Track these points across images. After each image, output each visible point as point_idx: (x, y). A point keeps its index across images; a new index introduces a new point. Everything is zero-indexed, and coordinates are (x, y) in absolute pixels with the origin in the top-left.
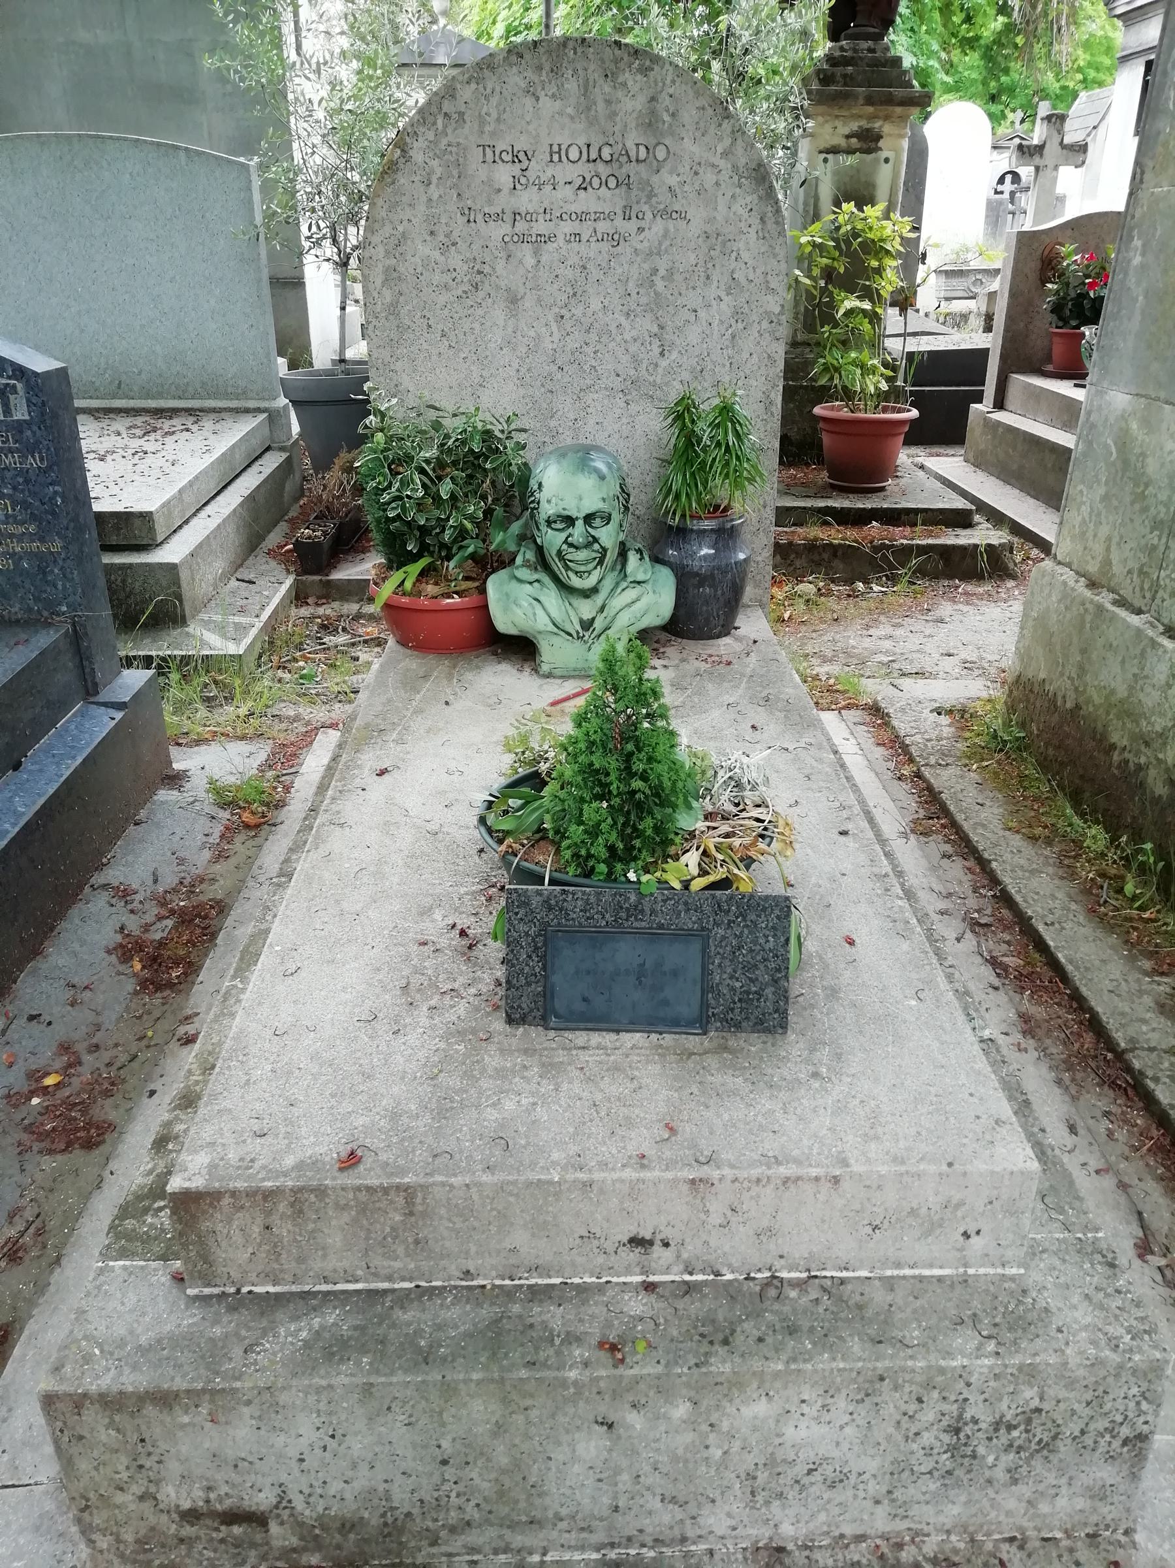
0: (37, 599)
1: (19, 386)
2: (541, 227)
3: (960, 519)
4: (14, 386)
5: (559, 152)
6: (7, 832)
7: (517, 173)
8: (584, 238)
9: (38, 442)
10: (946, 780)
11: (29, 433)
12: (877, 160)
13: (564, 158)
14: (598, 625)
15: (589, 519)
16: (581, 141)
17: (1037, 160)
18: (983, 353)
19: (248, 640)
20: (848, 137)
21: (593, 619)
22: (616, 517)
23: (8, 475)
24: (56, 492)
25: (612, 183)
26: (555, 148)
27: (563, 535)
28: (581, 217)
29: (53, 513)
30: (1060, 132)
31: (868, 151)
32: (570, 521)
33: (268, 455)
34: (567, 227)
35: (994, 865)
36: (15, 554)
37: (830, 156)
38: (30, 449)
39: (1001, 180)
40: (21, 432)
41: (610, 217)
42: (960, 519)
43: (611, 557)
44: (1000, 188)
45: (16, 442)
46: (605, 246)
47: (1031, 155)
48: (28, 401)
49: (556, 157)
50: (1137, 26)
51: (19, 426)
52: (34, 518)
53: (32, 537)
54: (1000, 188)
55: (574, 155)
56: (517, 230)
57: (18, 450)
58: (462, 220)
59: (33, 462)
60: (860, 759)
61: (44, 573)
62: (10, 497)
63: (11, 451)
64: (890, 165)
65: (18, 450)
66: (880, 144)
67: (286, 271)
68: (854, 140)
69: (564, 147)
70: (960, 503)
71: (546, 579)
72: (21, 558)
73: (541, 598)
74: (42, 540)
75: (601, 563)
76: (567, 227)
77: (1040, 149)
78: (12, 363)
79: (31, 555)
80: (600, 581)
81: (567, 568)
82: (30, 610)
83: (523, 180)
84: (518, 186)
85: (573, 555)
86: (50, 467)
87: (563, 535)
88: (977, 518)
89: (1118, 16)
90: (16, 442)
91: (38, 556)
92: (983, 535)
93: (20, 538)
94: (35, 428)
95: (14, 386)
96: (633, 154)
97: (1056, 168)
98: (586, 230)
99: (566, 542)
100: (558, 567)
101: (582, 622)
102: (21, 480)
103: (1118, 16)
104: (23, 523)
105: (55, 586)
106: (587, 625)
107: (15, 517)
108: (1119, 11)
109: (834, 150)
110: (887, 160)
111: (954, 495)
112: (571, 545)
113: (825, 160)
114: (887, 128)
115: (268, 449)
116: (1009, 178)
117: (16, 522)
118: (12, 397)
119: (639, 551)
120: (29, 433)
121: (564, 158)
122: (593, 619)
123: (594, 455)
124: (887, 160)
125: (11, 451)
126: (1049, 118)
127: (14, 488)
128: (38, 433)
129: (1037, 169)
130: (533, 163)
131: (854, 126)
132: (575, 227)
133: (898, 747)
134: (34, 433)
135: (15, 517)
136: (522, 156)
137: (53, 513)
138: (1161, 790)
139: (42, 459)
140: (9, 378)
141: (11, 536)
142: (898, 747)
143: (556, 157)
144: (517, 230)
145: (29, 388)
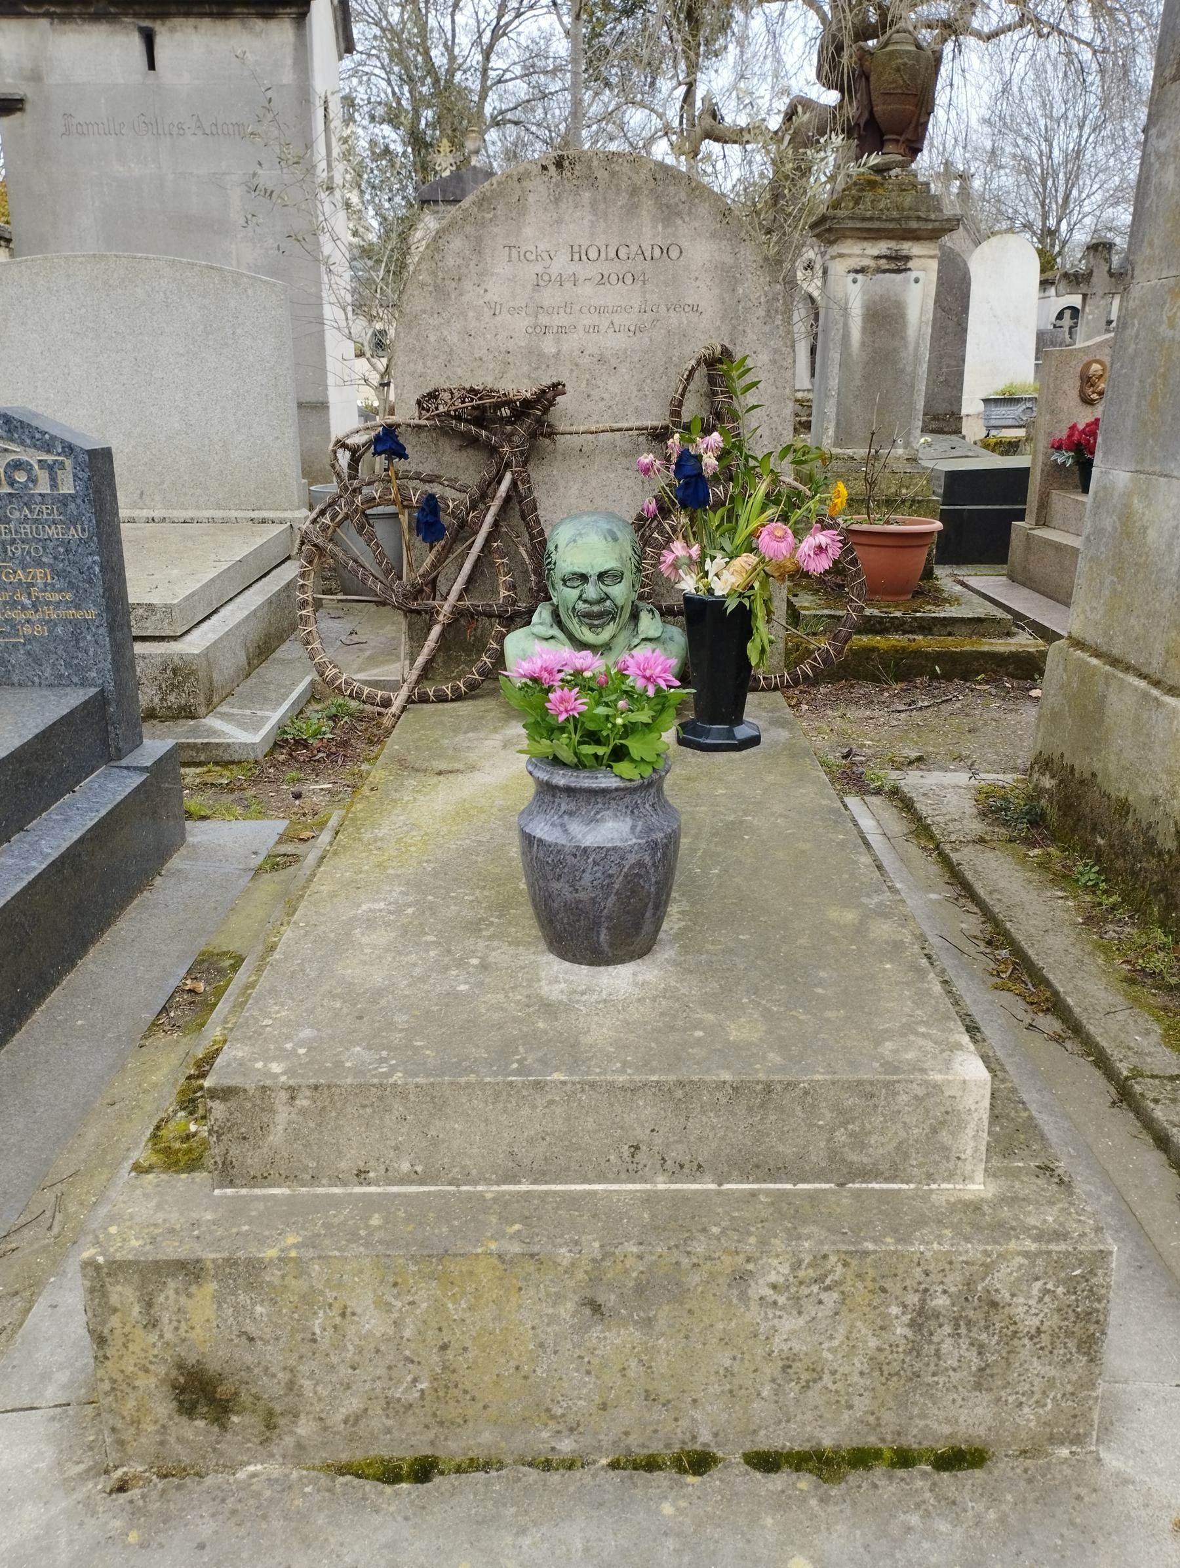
0: (68, 665)
2: (562, 319)
4: (62, 463)
6: (34, 868)
8: (603, 329)
9: (81, 514)
11: (73, 506)
12: (907, 281)
13: (584, 257)
15: (601, 576)
16: (600, 242)
17: (1083, 288)
18: (1025, 472)
19: (263, 732)
20: (877, 257)
22: (629, 577)
26: (576, 249)
27: (576, 592)
28: (600, 310)
29: (90, 581)
31: (898, 271)
32: (584, 578)
33: (289, 563)
34: (587, 320)
35: (1008, 925)
37: (860, 277)
39: (1060, 316)
40: (66, 505)
44: (1059, 323)
47: (1078, 283)
48: (75, 475)
49: (576, 257)
51: (64, 500)
52: (71, 585)
53: (69, 605)
54: (1059, 323)
55: (593, 254)
60: (880, 837)
61: (77, 640)
63: (54, 522)
66: (910, 264)
67: (310, 396)
68: (883, 261)
74: (78, 607)
79: (66, 622)
80: (614, 637)
87: (576, 592)
91: (75, 623)
92: (1023, 642)
94: (79, 501)
95: (62, 463)
96: (648, 254)
99: (580, 598)
102: (62, 550)
104: (61, 591)
107: (53, 585)
109: (862, 270)
110: (917, 281)
113: (855, 281)
114: (914, 248)
115: (289, 558)
116: (1068, 313)
119: (651, 611)
121: (584, 257)
124: (917, 281)
127: (55, 558)
129: (1085, 296)
132: (595, 319)
133: (921, 829)
134: (78, 506)
135: (53, 585)
138: (1171, 845)
139: (83, 530)
141: (48, 603)
142: (921, 829)
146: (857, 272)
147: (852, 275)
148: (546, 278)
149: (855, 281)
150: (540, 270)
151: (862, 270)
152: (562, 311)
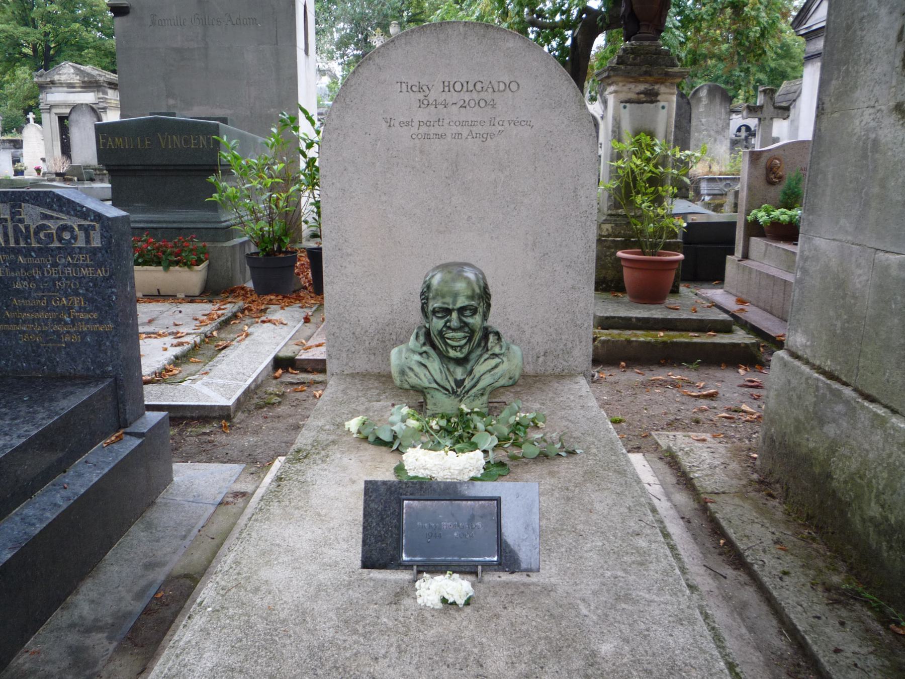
1: (97, 226)
3: (724, 328)
4: (94, 227)
5: (449, 86)
7: (422, 98)
8: (465, 135)
10: (729, 512)
11: (100, 255)
13: (452, 89)
14: (468, 384)
15: (461, 310)
20: (638, 94)
21: (464, 380)
23: (85, 281)
24: (113, 292)
25: (482, 104)
26: (446, 84)
28: (462, 124)
30: (772, 98)
31: (652, 102)
36: (83, 332)
37: (628, 105)
38: (100, 265)
40: (95, 254)
41: (482, 123)
42: (724, 328)
43: (477, 337)
45: (91, 260)
46: (478, 141)
49: (446, 89)
50: (813, 41)
51: (94, 252)
52: (97, 309)
53: (94, 321)
56: (420, 131)
57: (92, 266)
58: (385, 125)
59: (101, 273)
61: (100, 346)
62: (83, 295)
63: (87, 266)
64: (665, 111)
65: (92, 266)
66: (659, 98)
68: (642, 96)
69: (452, 83)
70: (724, 316)
71: (432, 352)
72: (86, 335)
73: (428, 364)
75: (470, 340)
76: (455, 129)
77: (761, 107)
78: (94, 212)
81: (446, 344)
82: (88, 369)
83: (426, 102)
84: (422, 106)
85: (450, 334)
86: (111, 276)
88: (734, 327)
89: (802, 35)
90: (91, 260)
91: (98, 334)
92: (740, 337)
93: (87, 321)
94: (104, 252)
95: (94, 227)
97: (772, 119)
98: (465, 131)
99: (445, 326)
100: (438, 342)
101: (456, 381)
103: (802, 35)
104: (89, 312)
105: (106, 353)
106: (459, 383)
107: (85, 308)
108: (802, 32)
109: (629, 101)
110: (663, 107)
111: (718, 311)
112: (449, 328)
113: (625, 107)
114: (663, 89)
116: (743, 129)
117: (86, 311)
118: (92, 232)
120: (100, 255)
121: (452, 89)
122: (464, 380)
123: (466, 269)
124: (663, 107)
125: (87, 266)
126: (764, 91)
127: (87, 290)
128: (106, 255)
129: (760, 119)
130: (432, 91)
131: (642, 87)
133: (685, 481)
135: (85, 308)
136: (425, 88)
137: (109, 306)
139: (106, 271)
140: (91, 221)
143: (446, 89)
144: (420, 131)
145: (103, 227)
146: (626, 102)
147: (623, 105)
148: (426, 102)
149: (625, 107)
150: (422, 98)
151: (629, 101)
152: (436, 124)
